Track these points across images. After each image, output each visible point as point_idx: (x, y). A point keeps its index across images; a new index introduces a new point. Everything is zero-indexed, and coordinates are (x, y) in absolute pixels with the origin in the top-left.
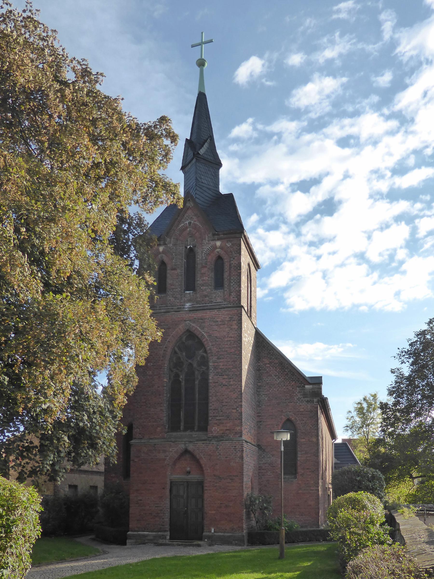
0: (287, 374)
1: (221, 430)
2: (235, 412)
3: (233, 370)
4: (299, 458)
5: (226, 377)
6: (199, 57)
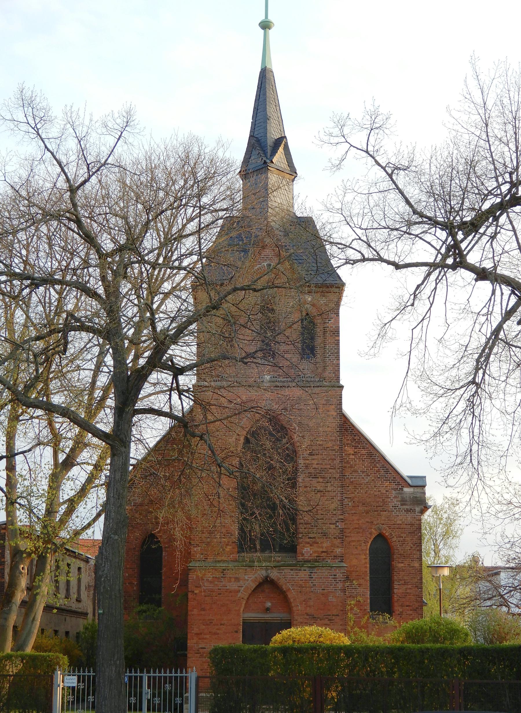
0: (378, 471)
1: (315, 552)
2: (334, 528)
3: (330, 470)
4: (395, 591)
5: (321, 480)
6: (263, 18)
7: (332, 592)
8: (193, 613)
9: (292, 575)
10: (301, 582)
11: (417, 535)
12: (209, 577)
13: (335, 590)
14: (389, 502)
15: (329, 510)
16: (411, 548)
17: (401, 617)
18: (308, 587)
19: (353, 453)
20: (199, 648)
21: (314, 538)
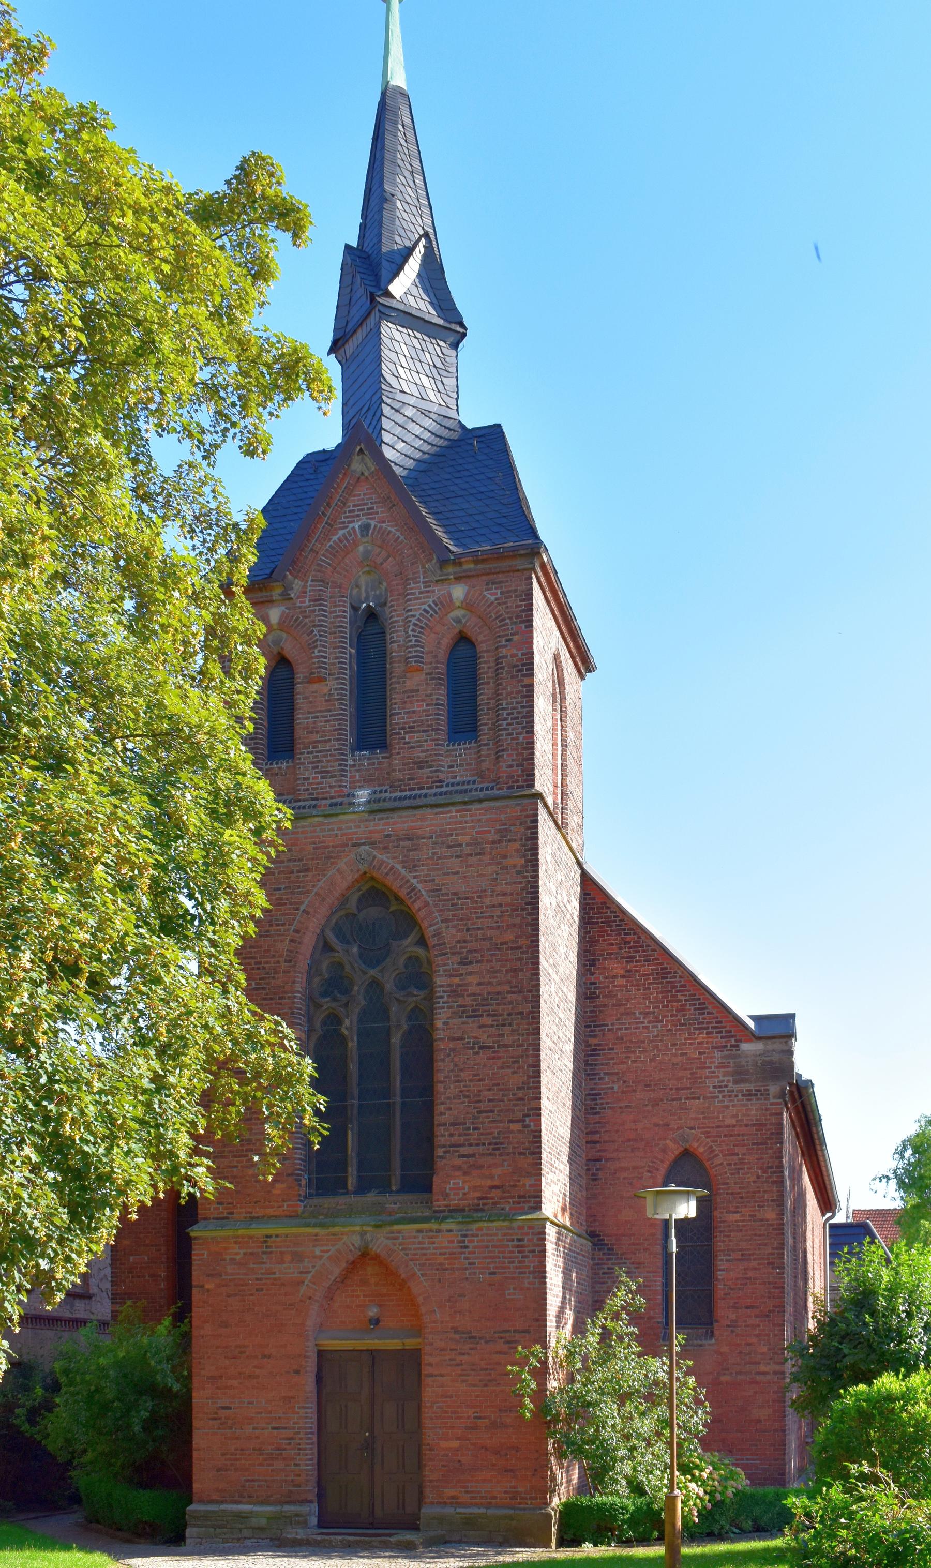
1: (475, 1188)
2: (520, 1132)
4: (720, 1275)
5: (488, 1021)
7: (513, 1278)
8: (202, 1332)
9: (420, 1243)
10: (441, 1259)
11: (771, 1148)
12: (237, 1254)
13: (521, 1273)
14: (707, 1077)
15: (509, 1090)
16: (758, 1177)
17: (732, 1331)
18: (459, 1269)
19: (623, 972)
20: (218, 1409)
21: (473, 1155)
